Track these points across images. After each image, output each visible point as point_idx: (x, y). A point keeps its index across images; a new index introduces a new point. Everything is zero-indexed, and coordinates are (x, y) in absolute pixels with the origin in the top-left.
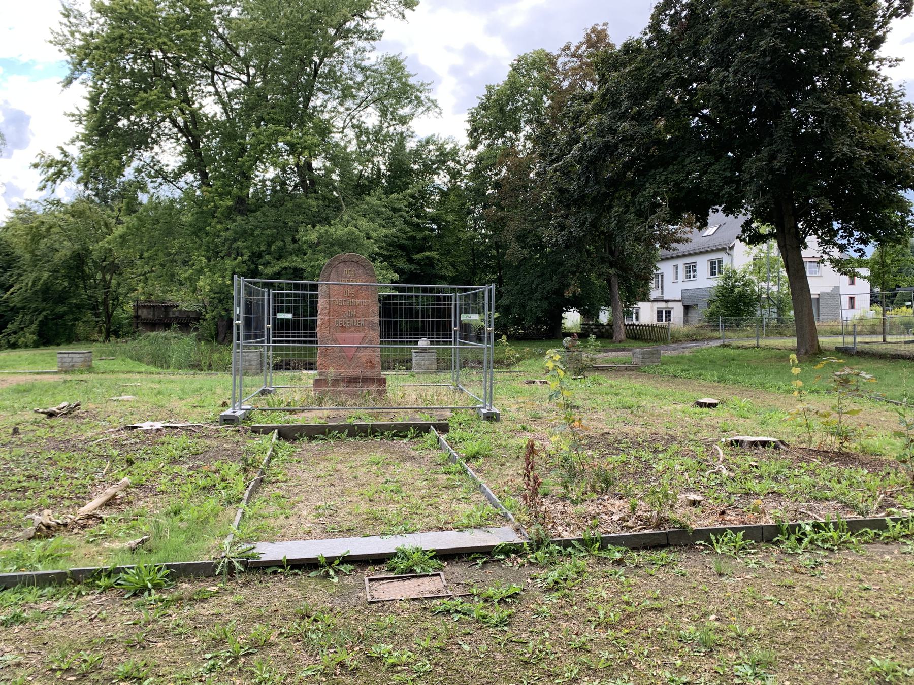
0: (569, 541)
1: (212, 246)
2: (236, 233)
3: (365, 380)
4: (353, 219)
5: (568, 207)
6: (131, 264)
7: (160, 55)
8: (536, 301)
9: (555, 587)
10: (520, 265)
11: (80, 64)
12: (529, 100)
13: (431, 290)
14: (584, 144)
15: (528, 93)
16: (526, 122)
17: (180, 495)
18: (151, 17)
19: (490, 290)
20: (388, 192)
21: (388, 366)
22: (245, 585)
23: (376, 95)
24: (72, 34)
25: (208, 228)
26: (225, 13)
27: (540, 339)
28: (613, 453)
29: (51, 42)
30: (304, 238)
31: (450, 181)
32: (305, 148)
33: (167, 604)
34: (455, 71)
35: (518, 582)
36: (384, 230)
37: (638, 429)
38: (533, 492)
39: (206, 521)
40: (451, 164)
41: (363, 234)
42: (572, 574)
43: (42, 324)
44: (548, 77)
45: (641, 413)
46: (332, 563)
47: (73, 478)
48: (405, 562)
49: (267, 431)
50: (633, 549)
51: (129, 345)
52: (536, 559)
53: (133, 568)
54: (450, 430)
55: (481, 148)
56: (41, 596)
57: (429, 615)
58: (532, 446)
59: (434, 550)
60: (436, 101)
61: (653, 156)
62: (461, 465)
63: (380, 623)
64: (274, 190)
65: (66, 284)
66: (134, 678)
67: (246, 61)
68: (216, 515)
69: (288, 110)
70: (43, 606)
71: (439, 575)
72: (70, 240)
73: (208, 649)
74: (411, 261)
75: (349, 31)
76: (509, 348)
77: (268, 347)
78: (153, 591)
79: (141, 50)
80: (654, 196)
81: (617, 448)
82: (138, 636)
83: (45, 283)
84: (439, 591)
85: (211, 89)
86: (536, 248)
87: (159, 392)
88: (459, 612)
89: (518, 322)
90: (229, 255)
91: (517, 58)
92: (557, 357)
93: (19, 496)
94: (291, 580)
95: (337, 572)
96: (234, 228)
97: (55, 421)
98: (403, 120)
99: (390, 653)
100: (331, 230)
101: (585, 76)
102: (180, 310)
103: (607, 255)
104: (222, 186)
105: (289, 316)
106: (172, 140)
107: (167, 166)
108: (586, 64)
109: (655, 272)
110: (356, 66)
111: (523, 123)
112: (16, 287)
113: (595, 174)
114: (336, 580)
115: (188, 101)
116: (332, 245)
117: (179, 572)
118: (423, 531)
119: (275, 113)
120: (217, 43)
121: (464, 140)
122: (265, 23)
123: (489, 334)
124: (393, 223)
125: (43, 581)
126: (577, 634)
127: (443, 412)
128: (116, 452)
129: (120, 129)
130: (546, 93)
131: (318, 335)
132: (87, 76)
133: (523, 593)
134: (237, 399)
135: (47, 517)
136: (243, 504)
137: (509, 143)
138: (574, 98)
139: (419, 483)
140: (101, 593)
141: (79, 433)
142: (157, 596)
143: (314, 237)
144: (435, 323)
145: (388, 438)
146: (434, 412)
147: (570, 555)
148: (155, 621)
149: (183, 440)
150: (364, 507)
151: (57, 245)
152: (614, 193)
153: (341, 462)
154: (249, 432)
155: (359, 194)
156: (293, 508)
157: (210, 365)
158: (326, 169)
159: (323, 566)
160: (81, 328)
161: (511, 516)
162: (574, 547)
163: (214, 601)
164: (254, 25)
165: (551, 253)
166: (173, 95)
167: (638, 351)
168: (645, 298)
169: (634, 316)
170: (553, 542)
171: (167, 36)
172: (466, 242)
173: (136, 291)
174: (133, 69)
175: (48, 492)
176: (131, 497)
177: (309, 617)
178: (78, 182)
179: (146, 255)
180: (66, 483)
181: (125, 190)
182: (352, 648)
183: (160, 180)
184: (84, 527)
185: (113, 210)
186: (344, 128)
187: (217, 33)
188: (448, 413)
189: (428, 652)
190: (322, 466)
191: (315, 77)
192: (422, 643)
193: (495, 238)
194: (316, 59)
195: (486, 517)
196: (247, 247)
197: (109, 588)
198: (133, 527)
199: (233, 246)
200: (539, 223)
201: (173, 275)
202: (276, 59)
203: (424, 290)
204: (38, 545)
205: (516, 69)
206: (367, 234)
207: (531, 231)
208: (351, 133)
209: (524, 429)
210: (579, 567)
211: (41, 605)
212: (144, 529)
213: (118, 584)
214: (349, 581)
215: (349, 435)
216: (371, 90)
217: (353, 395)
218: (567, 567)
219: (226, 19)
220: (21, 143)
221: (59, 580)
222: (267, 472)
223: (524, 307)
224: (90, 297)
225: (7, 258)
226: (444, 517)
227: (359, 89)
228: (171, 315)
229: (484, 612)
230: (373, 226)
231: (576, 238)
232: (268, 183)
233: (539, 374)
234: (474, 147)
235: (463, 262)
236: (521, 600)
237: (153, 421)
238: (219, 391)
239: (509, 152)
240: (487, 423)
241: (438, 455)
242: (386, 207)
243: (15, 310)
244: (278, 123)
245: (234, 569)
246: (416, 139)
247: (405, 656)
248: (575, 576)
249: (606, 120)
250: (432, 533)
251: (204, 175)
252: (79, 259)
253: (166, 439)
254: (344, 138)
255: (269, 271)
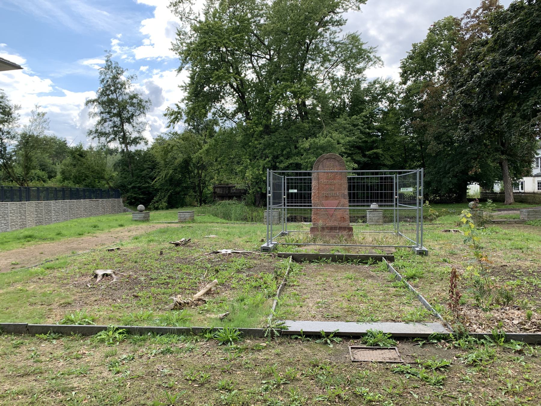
0: (482, 335)
1: (252, 153)
2: (265, 145)
3: (340, 228)
4: (330, 133)
5: (471, 116)
6: (211, 165)
7: (224, 50)
8: (448, 178)
9: (474, 364)
10: (437, 155)
11: (186, 59)
12: (442, 50)
13: (377, 174)
14: (482, 74)
15: (441, 46)
16: (440, 64)
17: (243, 290)
18: (220, 30)
19: (420, 172)
20: (350, 115)
21: (354, 219)
22: (280, 344)
23: (343, 58)
24: (182, 44)
25: (250, 143)
26: (257, 22)
27: (451, 203)
28: (511, 279)
29: (172, 49)
30: (302, 146)
31: (389, 105)
32: (302, 93)
33: (241, 350)
34: (390, 38)
35: (447, 358)
36: (348, 138)
37: (528, 263)
38: (456, 302)
39: (257, 306)
40: (390, 95)
41: (336, 141)
42: (486, 357)
43: (170, 197)
44: (455, 33)
45: (529, 252)
46: (329, 336)
47: (190, 279)
48: (373, 339)
49: (286, 256)
50: (530, 344)
51: (211, 208)
52: (459, 344)
53: (222, 329)
54: (395, 260)
55: (409, 83)
56: (179, 340)
57: (390, 373)
58: (455, 273)
59: (390, 334)
60: (380, 57)
61: (534, 78)
62: (404, 282)
63: (360, 374)
64: (284, 120)
65: (180, 176)
66: (227, 389)
67: (268, 47)
68: (263, 303)
69: (292, 73)
70: (180, 345)
71: (394, 349)
72: (182, 153)
73: (263, 378)
74: (364, 156)
75: (327, 22)
76: (431, 209)
77: (284, 209)
78: (233, 343)
79: (215, 48)
80: (535, 104)
81: (513, 276)
82: (227, 366)
83: (171, 176)
84: (395, 359)
85: (250, 65)
86: (448, 144)
87: (228, 234)
88: (410, 373)
89: (436, 192)
90: (261, 158)
91: (433, 24)
92: (470, 215)
93: (165, 287)
94: (305, 343)
95: (332, 341)
96: (267, 140)
97: (181, 248)
98: (359, 71)
99: (367, 393)
100: (317, 140)
101: (481, 30)
102: (236, 189)
103: (500, 146)
104: (258, 120)
105: (296, 191)
106: (231, 96)
107: (229, 110)
108: (482, 22)
109: (536, 156)
110: (331, 42)
111: (437, 65)
112: (157, 178)
113: (490, 93)
114: (331, 346)
115: (239, 74)
116: (317, 149)
117: (246, 334)
118: (383, 321)
119: (285, 75)
120: (253, 39)
121: (398, 79)
122: (279, 24)
123: (420, 200)
124: (354, 134)
125: (180, 332)
126: (492, 397)
127: (390, 249)
128: (209, 266)
129: (205, 92)
130: (453, 44)
131: (312, 202)
132: (189, 65)
133: (451, 366)
134: (269, 238)
135: (179, 298)
136: (276, 297)
137: (428, 79)
138: (474, 44)
139: (378, 292)
140: (207, 341)
141: (191, 255)
142: (235, 346)
143: (307, 145)
144: (383, 194)
145: (356, 263)
146: (384, 248)
147: (483, 344)
148: (235, 359)
149: (242, 260)
150: (345, 304)
151: (176, 156)
152: (504, 105)
153: (329, 276)
154: (277, 257)
155: (333, 118)
156: (304, 302)
157: (252, 219)
158: (313, 104)
159: (323, 337)
160: (188, 199)
161: (440, 316)
162: (485, 339)
163: (264, 351)
164: (274, 27)
165: (458, 147)
166: (231, 71)
167: (524, 210)
168: (528, 174)
169: (520, 186)
170: (471, 335)
171: (228, 39)
172: (400, 142)
173: (215, 179)
174: (211, 59)
175: (178, 285)
176: (219, 291)
177: (318, 366)
178: (185, 122)
179: (219, 159)
180: (187, 281)
181: (208, 125)
182: (344, 387)
183: (225, 118)
184: (196, 305)
185: (202, 136)
186: (324, 79)
187: (253, 33)
188: (393, 250)
189: (391, 396)
190: (318, 278)
191: (307, 52)
192: (387, 390)
193: (419, 139)
194: (308, 41)
195: (424, 315)
196: (270, 153)
197: (210, 339)
198: (220, 307)
199: (264, 152)
200: (450, 128)
201: (232, 170)
202: (284, 44)
203: (373, 174)
204: (176, 313)
205: (432, 31)
206: (338, 141)
207: (444, 133)
208: (328, 82)
209: (445, 261)
210: (490, 353)
211: (179, 345)
212: (226, 308)
213: (215, 337)
214: (339, 347)
215: (332, 261)
216: (340, 55)
217: (333, 237)
218: (481, 352)
219: (259, 26)
220: (158, 104)
221: (186, 332)
222: (288, 280)
223: (440, 182)
224: (192, 183)
225: (153, 163)
226: (396, 314)
227: (332, 56)
228: (232, 191)
229: (426, 375)
230: (341, 136)
231: (477, 136)
232: (281, 116)
233: (453, 226)
234: (405, 83)
235: (398, 155)
236: (451, 370)
237: (227, 249)
238: (259, 233)
239: (428, 84)
240: (420, 257)
241: (388, 275)
242: (349, 124)
243: (157, 190)
244: (287, 80)
245: (274, 334)
246: (367, 82)
247: (377, 396)
248: (488, 358)
249: (497, 55)
250: (388, 323)
251: (247, 114)
252: (187, 162)
253: (234, 259)
254: (324, 85)
255: (282, 166)
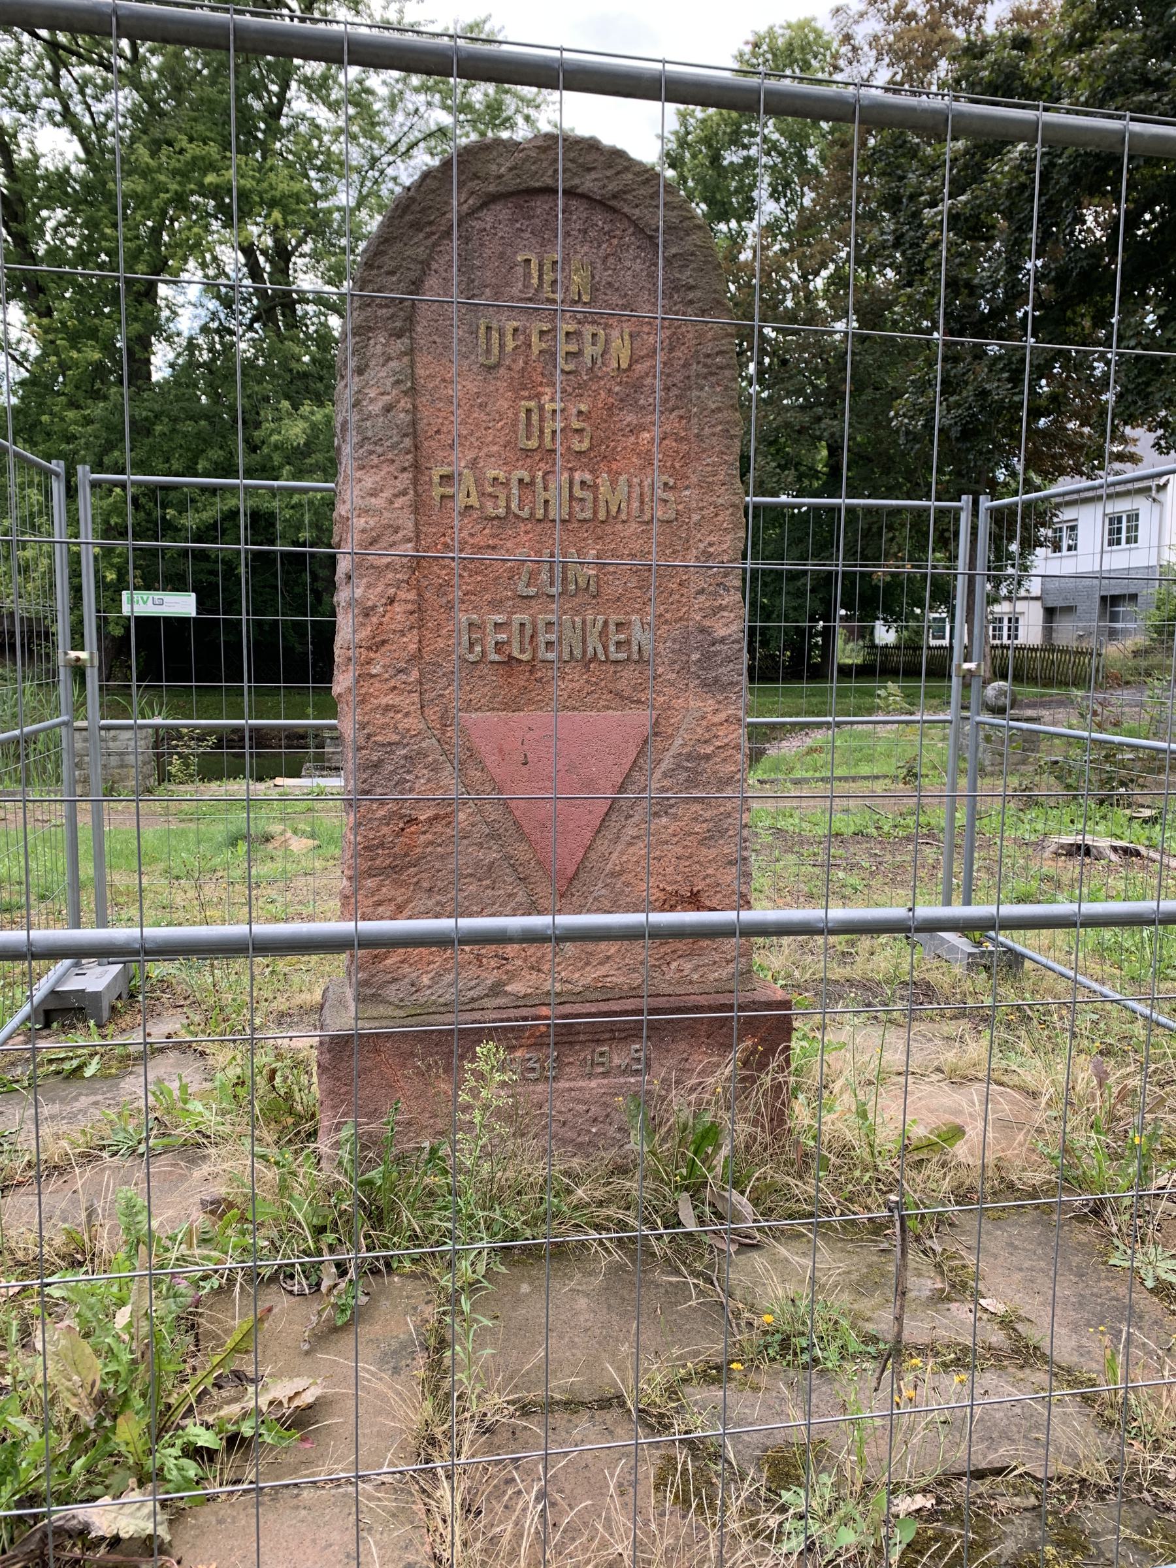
30: (275, 438)
91: (751, 38)
143: (297, 430)
